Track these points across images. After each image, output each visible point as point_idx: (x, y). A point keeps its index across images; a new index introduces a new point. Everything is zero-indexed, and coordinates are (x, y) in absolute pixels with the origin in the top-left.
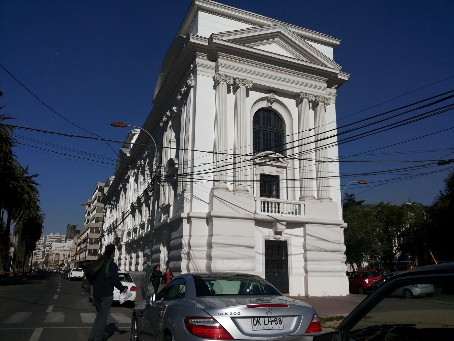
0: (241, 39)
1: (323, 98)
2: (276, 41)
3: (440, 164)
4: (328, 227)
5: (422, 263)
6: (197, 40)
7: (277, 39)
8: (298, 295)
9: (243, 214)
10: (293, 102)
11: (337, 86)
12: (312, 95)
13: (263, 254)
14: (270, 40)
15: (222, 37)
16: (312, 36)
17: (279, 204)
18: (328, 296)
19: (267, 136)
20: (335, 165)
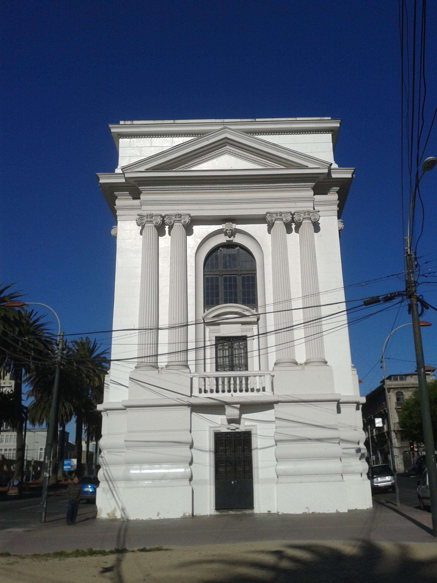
0: (169, 163)
1: (306, 213)
2: (226, 151)
3: (367, 303)
4: (318, 405)
5: (33, 475)
6: (109, 179)
7: (227, 147)
8: (267, 512)
9: (173, 398)
10: (264, 227)
11: (339, 188)
12: (287, 213)
13: (210, 451)
14: (217, 152)
15: (137, 168)
16: (291, 127)
17: (247, 378)
18: (313, 513)
19: (230, 281)
20: (339, 307)
